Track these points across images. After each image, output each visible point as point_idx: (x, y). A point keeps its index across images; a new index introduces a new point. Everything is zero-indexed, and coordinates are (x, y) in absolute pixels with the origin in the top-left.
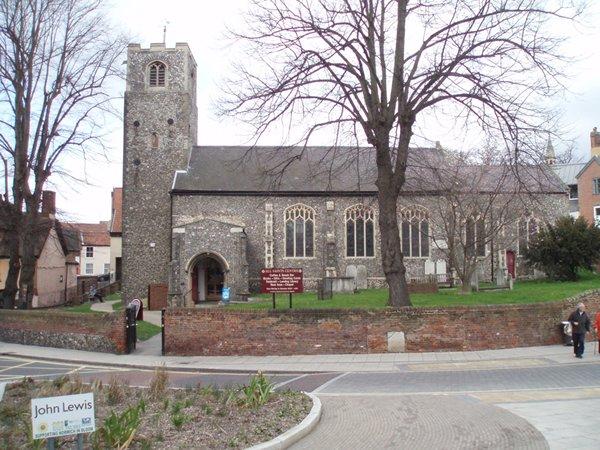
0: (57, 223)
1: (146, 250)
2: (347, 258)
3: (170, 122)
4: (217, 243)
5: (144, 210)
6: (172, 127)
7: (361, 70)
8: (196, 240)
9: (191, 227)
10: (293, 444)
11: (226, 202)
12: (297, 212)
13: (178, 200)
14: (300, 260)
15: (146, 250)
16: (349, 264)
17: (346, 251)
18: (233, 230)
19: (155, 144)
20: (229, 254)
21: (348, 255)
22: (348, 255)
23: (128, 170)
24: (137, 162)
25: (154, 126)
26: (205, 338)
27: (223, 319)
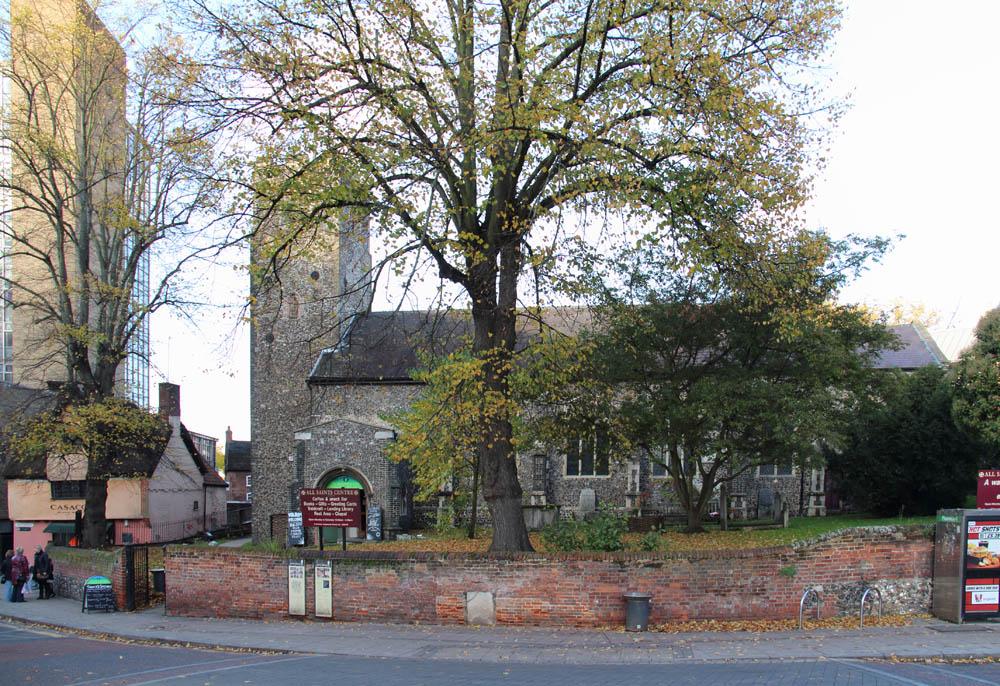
0: (187, 437)
1: (283, 465)
2: (566, 477)
3: (315, 275)
5: (280, 408)
6: (317, 285)
7: (469, 166)
8: (328, 447)
10: (968, 631)
11: (388, 394)
15: (283, 465)
16: (584, 487)
17: (565, 467)
18: (379, 435)
19: (294, 312)
20: (373, 471)
21: (569, 473)
22: (569, 473)
23: (257, 349)
24: (270, 338)
25: (293, 283)
26: (216, 591)
27: (238, 564)
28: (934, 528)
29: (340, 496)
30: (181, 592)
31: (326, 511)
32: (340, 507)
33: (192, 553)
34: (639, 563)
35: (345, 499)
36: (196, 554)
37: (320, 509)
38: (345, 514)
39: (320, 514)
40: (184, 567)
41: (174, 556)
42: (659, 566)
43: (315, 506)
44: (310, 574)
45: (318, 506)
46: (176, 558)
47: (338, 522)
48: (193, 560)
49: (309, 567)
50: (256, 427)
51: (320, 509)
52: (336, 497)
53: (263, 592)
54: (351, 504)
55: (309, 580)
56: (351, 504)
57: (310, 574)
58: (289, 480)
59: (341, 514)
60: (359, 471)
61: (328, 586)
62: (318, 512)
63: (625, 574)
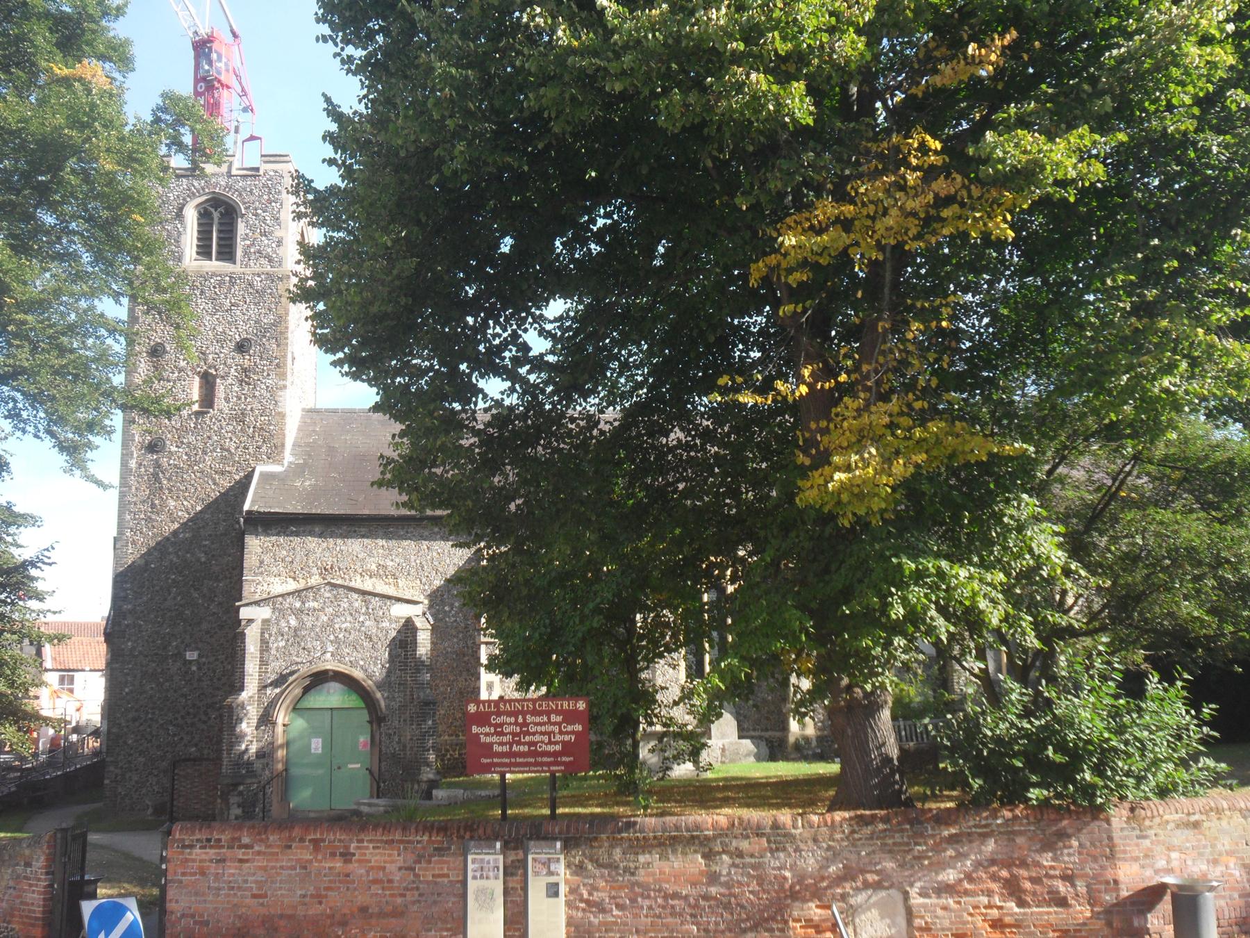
27: (347, 856)
28: (416, 809)
29: (548, 713)
30: (207, 923)
31: (519, 743)
32: (549, 734)
33: (239, 839)
34: (1167, 822)
35: (559, 719)
36: (246, 840)
37: (505, 739)
38: (558, 748)
39: (506, 749)
40: (213, 869)
41: (191, 847)
42: (1196, 825)
43: (497, 734)
44: (515, 875)
45: (502, 734)
46: (197, 851)
47: (542, 764)
48: (240, 854)
49: (512, 856)
50: (125, 599)
51: (505, 739)
52: (540, 714)
53: (402, 914)
54: (570, 728)
55: (515, 882)
56: (570, 728)
57: (515, 875)
58: (184, 696)
59: (551, 748)
61: (556, 894)
62: (502, 744)
63: (1147, 843)
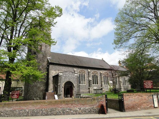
4: (71, 78)
8: (65, 77)
9: (64, 73)
12: (81, 72)
13: (51, 66)
14: (82, 85)
27: (142, 97)
60: (72, 82)
